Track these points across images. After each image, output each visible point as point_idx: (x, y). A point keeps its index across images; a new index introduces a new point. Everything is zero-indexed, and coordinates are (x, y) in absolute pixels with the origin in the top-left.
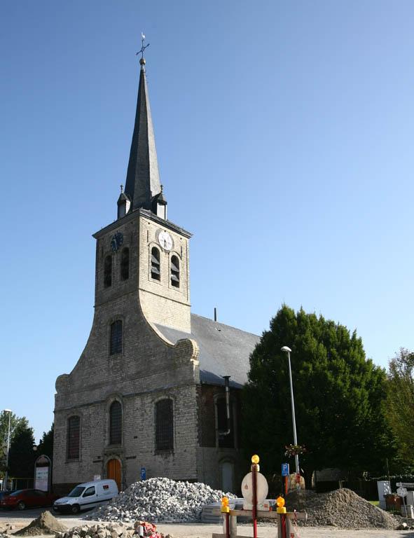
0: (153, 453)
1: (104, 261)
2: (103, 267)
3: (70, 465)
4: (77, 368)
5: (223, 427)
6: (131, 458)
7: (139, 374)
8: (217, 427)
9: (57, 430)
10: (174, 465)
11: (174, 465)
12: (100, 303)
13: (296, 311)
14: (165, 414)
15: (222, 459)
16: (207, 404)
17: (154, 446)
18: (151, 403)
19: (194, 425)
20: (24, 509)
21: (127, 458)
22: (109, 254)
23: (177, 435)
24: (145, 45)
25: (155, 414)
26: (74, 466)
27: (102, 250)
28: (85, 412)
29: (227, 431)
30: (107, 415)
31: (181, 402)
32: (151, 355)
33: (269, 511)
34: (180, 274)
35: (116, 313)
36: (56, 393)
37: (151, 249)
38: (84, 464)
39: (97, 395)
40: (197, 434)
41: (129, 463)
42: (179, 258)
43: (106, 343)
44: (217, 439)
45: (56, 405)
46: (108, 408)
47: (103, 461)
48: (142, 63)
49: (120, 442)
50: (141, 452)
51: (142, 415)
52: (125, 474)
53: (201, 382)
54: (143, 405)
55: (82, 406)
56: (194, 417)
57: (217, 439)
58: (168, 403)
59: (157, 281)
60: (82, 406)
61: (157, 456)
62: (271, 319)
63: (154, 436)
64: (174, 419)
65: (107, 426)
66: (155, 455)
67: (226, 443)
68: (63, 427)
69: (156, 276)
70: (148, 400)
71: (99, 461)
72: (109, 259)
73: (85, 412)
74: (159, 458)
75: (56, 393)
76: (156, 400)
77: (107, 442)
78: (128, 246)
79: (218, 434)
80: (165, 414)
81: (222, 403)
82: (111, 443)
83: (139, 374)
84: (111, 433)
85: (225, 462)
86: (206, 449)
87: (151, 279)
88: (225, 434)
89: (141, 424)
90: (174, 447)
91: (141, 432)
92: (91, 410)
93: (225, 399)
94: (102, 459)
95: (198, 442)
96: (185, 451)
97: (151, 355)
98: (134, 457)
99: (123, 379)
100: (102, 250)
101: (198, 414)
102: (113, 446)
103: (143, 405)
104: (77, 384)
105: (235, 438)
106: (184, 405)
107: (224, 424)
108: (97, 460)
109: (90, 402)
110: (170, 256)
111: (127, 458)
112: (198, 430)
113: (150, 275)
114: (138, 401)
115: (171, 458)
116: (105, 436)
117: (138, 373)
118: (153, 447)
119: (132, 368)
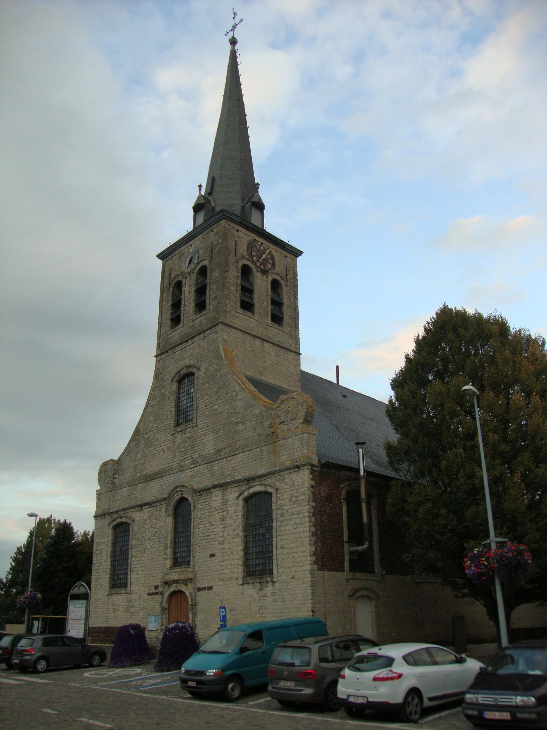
0: (241, 582)
1: (171, 290)
2: (170, 298)
3: (114, 597)
4: (128, 450)
5: (356, 537)
6: (204, 589)
7: (219, 455)
8: (346, 538)
9: (98, 543)
10: (275, 600)
11: (275, 600)
12: (164, 350)
13: (485, 316)
14: (259, 512)
15: (356, 591)
16: (329, 499)
17: (241, 569)
18: (238, 498)
19: (308, 534)
20: (47, 671)
21: (199, 589)
22: (180, 278)
23: (280, 551)
24: (237, 20)
25: (243, 515)
26: (120, 599)
27: (170, 274)
28: (137, 516)
29: (478, 551)
30: (170, 521)
31: (287, 496)
32: (237, 423)
33: (200, 193)
34: (285, 307)
35: (187, 362)
36: (99, 488)
37: (240, 266)
38: (134, 597)
39: (155, 490)
40: (313, 548)
41: (202, 596)
42: (282, 283)
43: (170, 407)
44: (347, 558)
45: (98, 506)
46: (172, 506)
47: (162, 593)
48: (233, 42)
49: (188, 563)
50: (220, 580)
51: (223, 519)
52: (195, 614)
53: (319, 461)
54: (225, 502)
55: (134, 507)
56: (307, 520)
57: (347, 558)
58: (265, 497)
59: (249, 314)
60: (134, 507)
61: (246, 587)
62: (439, 308)
63: (242, 554)
64: (274, 524)
65: (170, 537)
66: (243, 584)
67: (361, 564)
68: (106, 539)
69: (247, 306)
70: (232, 494)
71: (156, 594)
72: (179, 285)
73: (137, 516)
74: (250, 590)
75: (99, 488)
76: (246, 494)
77: (169, 563)
78: (206, 263)
79: (347, 548)
80: (259, 512)
81: (353, 498)
82: (177, 562)
83: (219, 455)
84: (175, 548)
85: (363, 596)
86: (327, 574)
87: (241, 311)
88: (360, 548)
89: (221, 534)
90: (275, 572)
91: (221, 546)
92: (146, 512)
93: (358, 492)
94: (160, 589)
95: (315, 562)
96: (293, 578)
97: (237, 423)
98: (210, 588)
99: (194, 463)
100: (170, 274)
101: (314, 515)
102: (177, 569)
103: (225, 502)
104: (127, 475)
105: (376, 556)
106: (290, 500)
107: (357, 534)
108: (154, 591)
109: (148, 500)
110: (270, 279)
111: (199, 589)
112: (315, 542)
113: (239, 304)
114: (217, 497)
115: (269, 589)
116: (165, 554)
117: (218, 451)
118: (239, 571)
119: (208, 444)
